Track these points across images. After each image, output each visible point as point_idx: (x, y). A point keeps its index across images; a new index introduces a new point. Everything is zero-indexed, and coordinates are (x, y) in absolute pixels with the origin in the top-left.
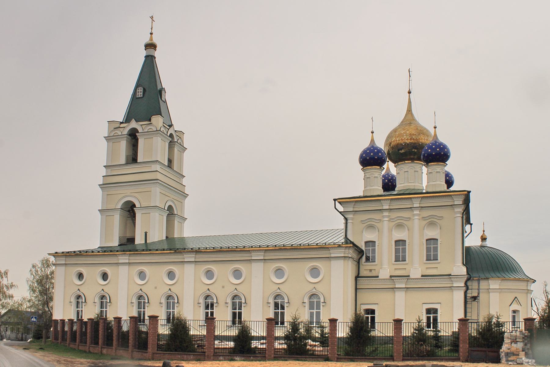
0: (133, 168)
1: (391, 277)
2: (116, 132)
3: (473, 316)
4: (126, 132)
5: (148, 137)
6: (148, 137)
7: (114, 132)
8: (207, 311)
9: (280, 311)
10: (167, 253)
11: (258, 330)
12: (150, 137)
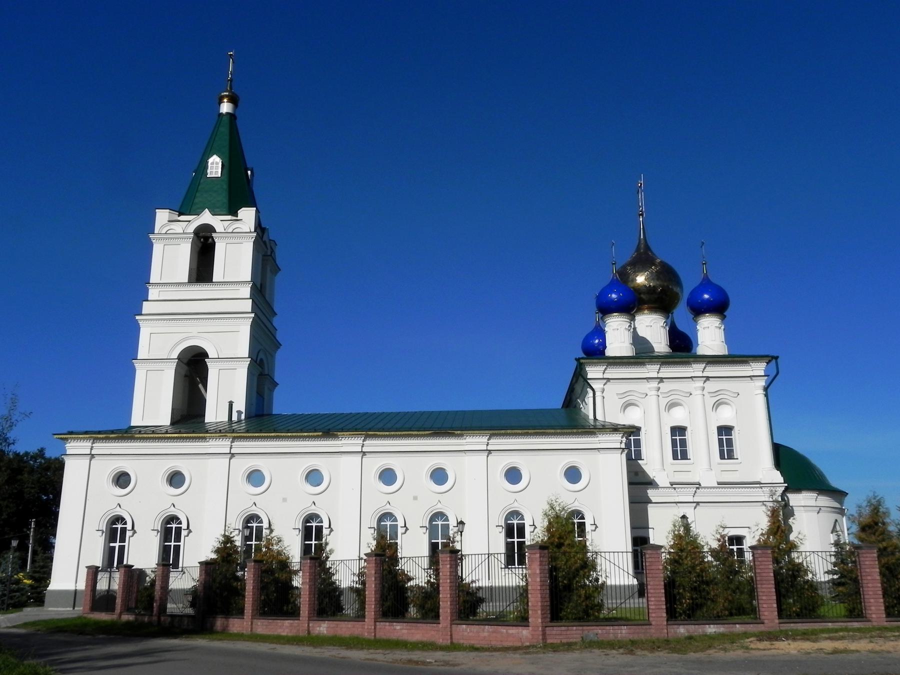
0: (202, 290)
1: (672, 484)
2: (172, 227)
3: (561, 563)
4: (192, 228)
5: (236, 241)
6: (236, 241)
7: (168, 228)
8: (112, 545)
9: (516, 540)
10: (174, 438)
11: (345, 578)
12: (238, 241)
